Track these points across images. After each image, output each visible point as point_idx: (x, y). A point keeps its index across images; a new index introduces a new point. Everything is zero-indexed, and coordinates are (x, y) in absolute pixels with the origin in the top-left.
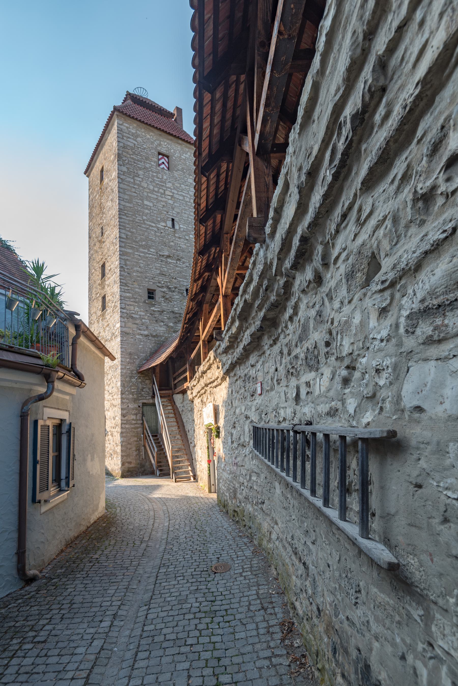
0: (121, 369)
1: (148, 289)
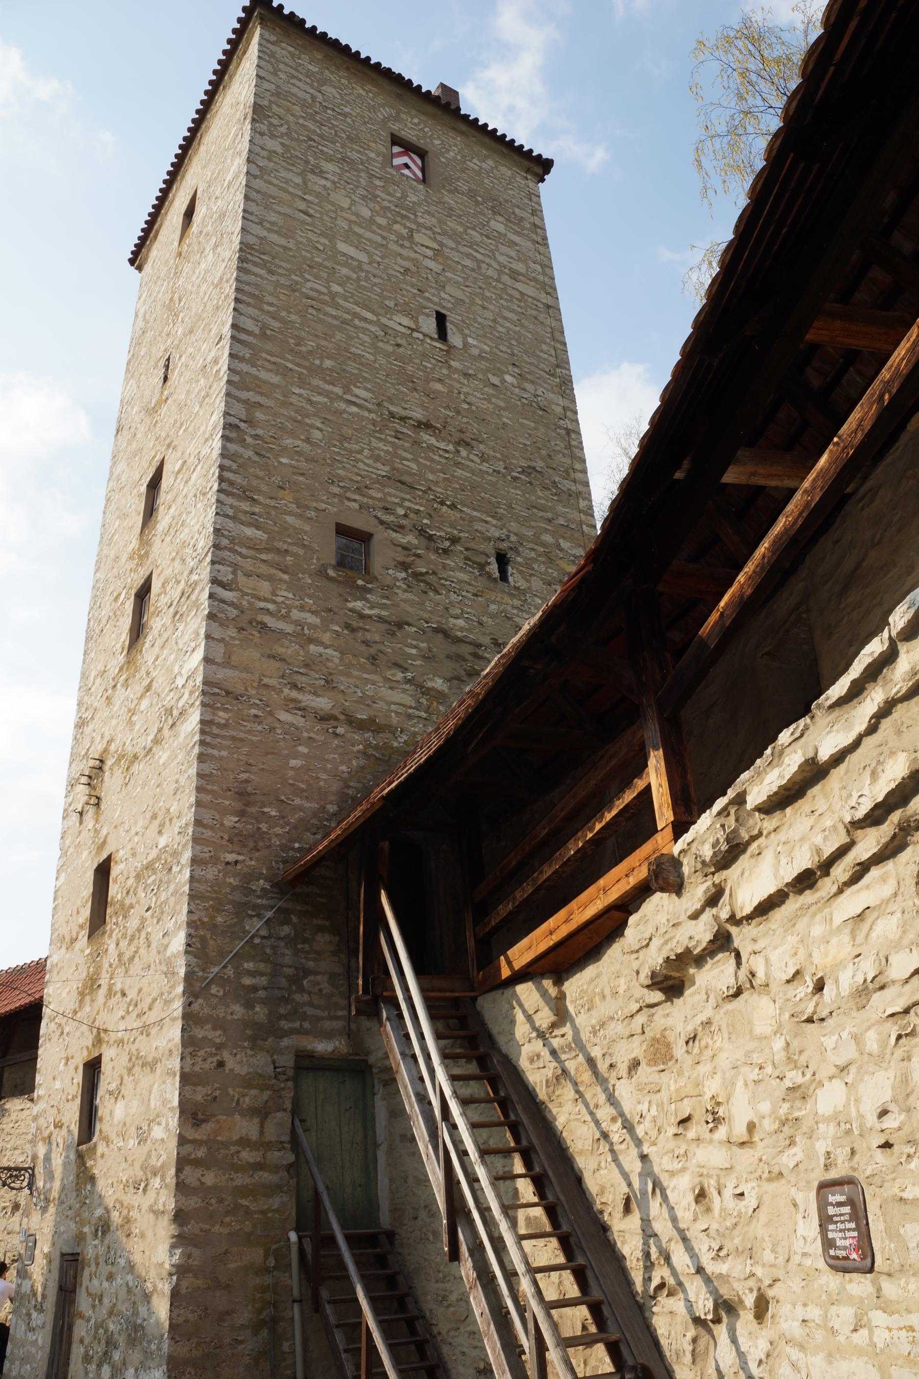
0: (194, 861)
1: (337, 524)
